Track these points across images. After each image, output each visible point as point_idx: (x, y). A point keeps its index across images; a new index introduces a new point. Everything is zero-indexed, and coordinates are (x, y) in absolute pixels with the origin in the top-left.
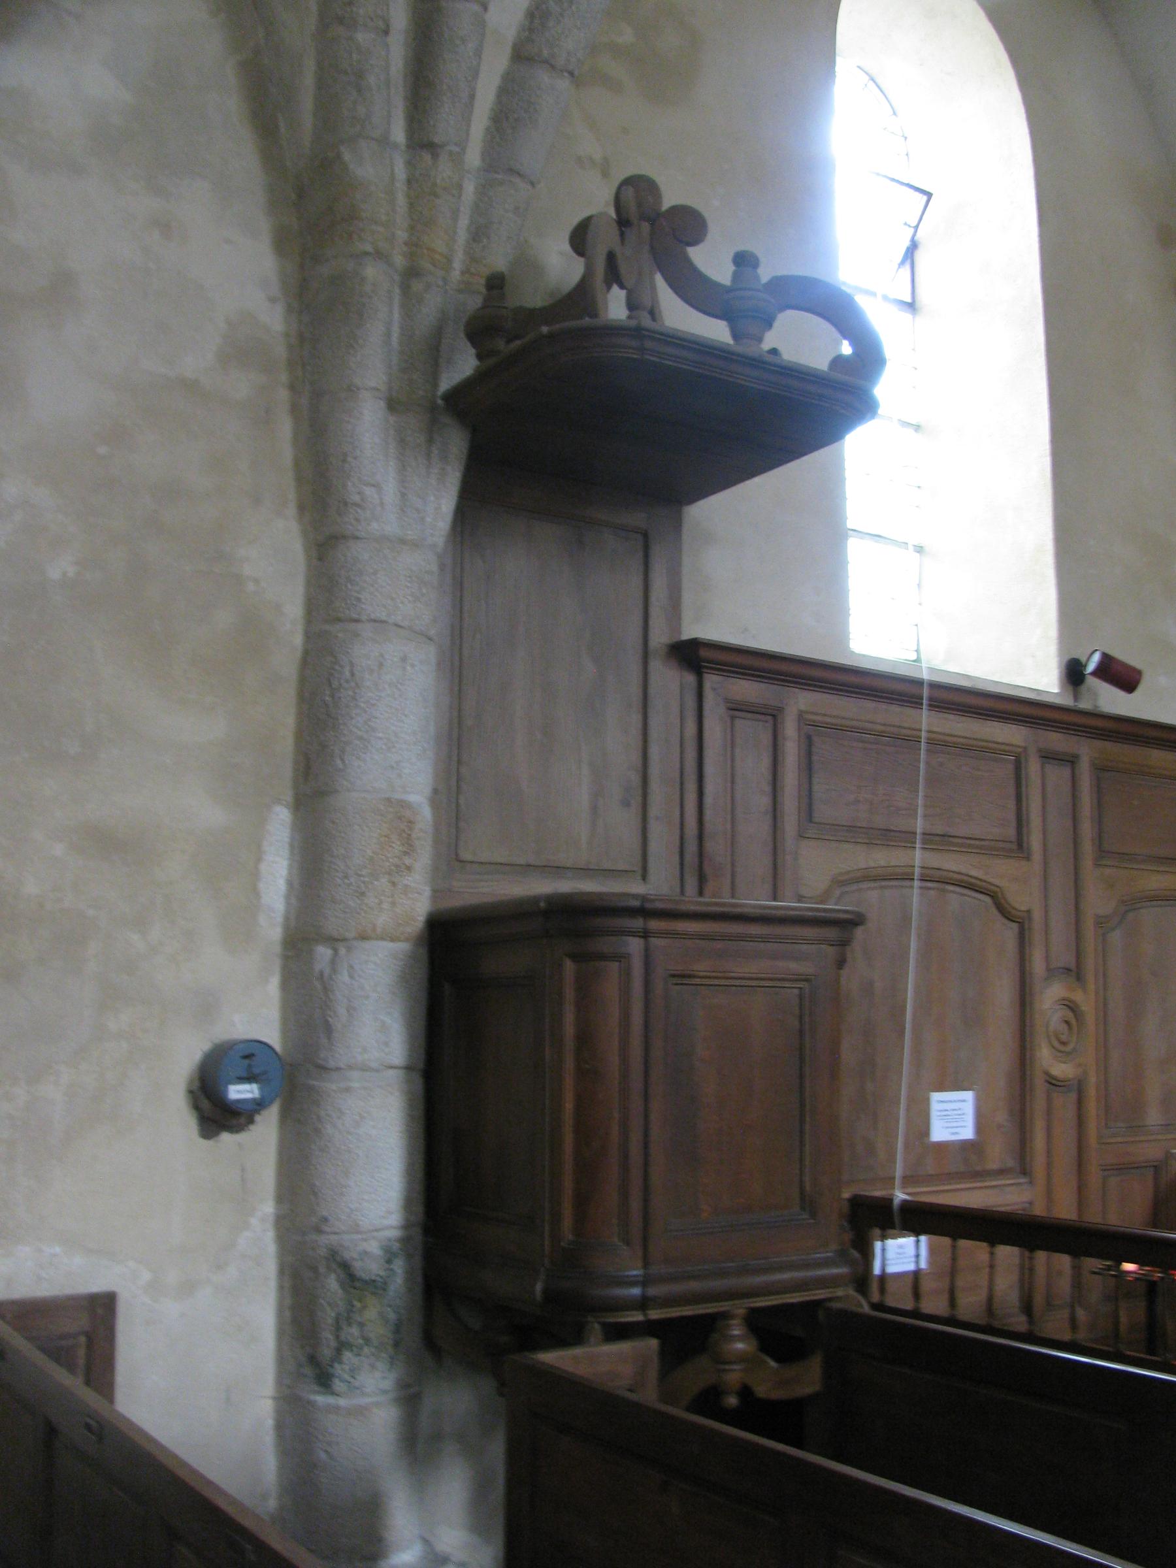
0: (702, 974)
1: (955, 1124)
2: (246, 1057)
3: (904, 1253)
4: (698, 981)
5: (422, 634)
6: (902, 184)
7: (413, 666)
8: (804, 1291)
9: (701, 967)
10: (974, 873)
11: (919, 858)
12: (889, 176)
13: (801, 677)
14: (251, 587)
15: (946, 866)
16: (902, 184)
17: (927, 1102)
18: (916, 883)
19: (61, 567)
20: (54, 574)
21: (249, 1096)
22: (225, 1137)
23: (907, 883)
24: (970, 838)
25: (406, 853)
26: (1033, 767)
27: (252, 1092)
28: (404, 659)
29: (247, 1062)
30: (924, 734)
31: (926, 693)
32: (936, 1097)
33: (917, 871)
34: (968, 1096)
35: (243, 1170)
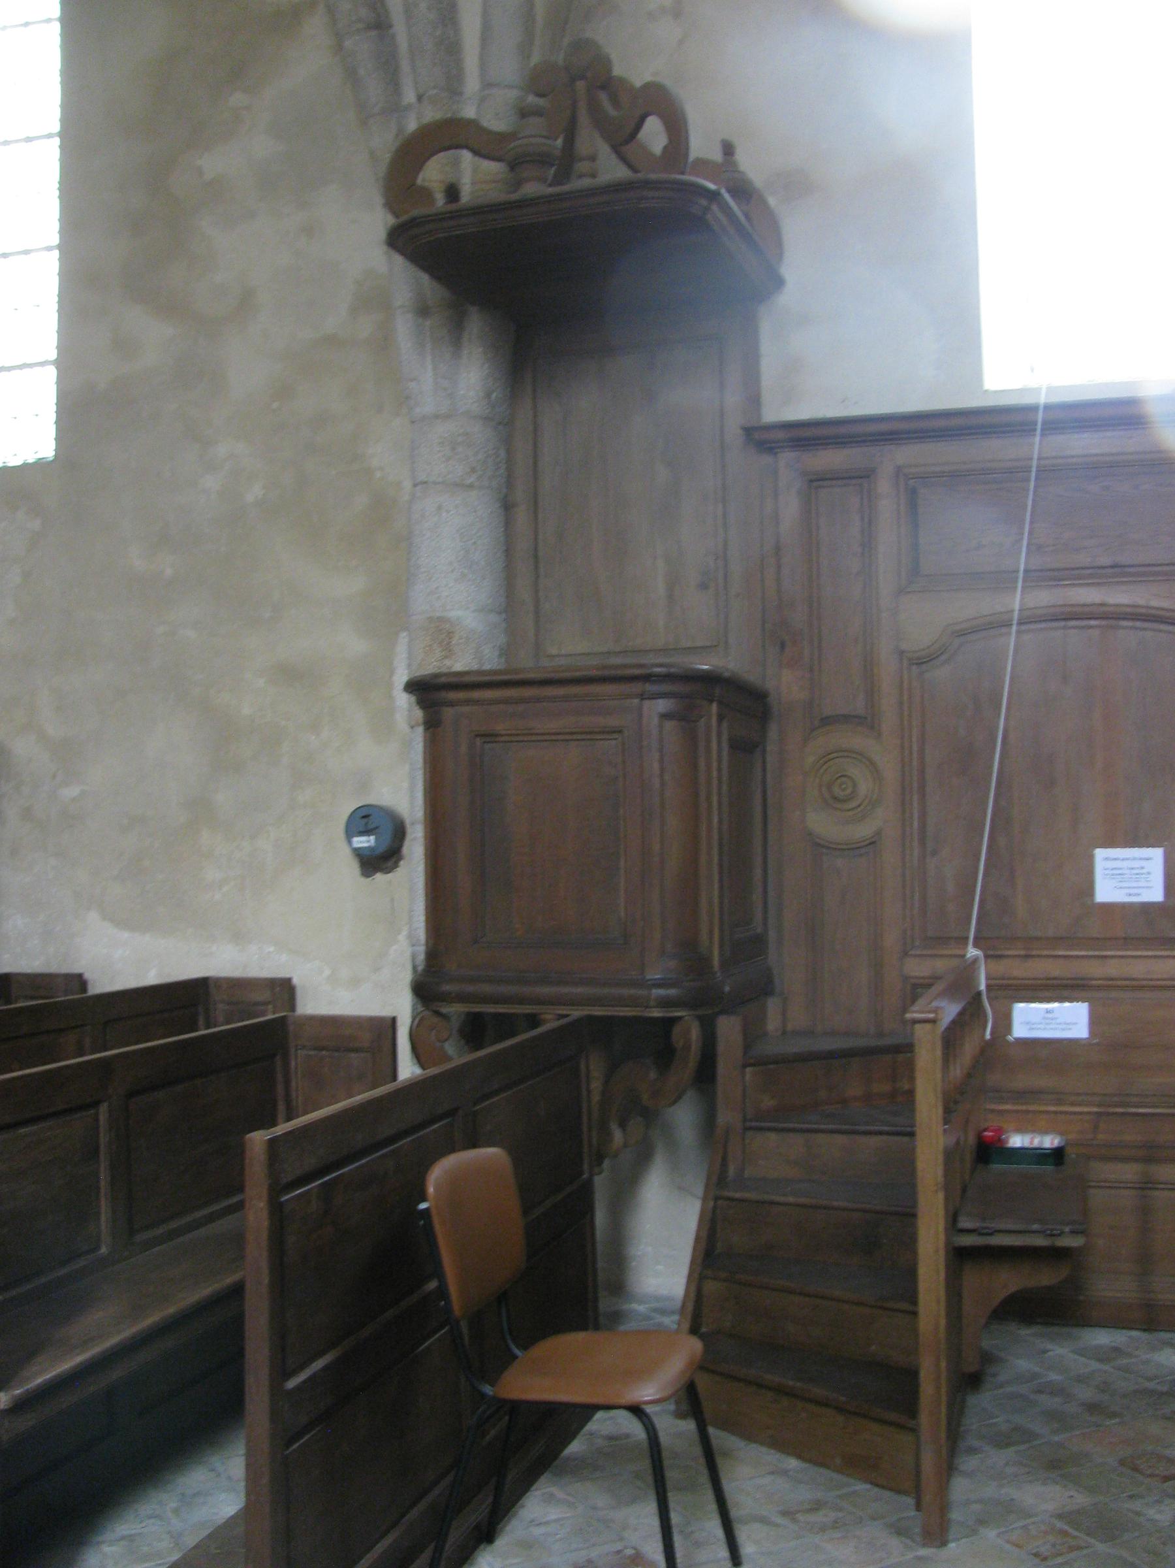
0: (504, 732)
1: (1135, 884)
2: (364, 817)
3: (1056, 1018)
4: (503, 739)
5: (456, 485)
6: (17, 26)
7: (448, 512)
8: (470, 1003)
9: (500, 728)
10: (1154, 603)
11: (1016, 602)
12: (20, 23)
13: (819, 438)
14: (378, 474)
15: (1111, 600)
16: (17, 26)
17: (1091, 859)
18: (1014, 628)
19: (254, 493)
20: (250, 498)
21: (366, 845)
22: (379, 876)
23: (1004, 630)
24: (1154, 565)
25: (446, 657)
27: (368, 841)
28: (440, 508)
29: (365, 820)
30: (1035, 463)
31: (1040, 417)
32: (1100, 854)
33: (1016, 615)
34: (1156, 855)
35: (392, 900)
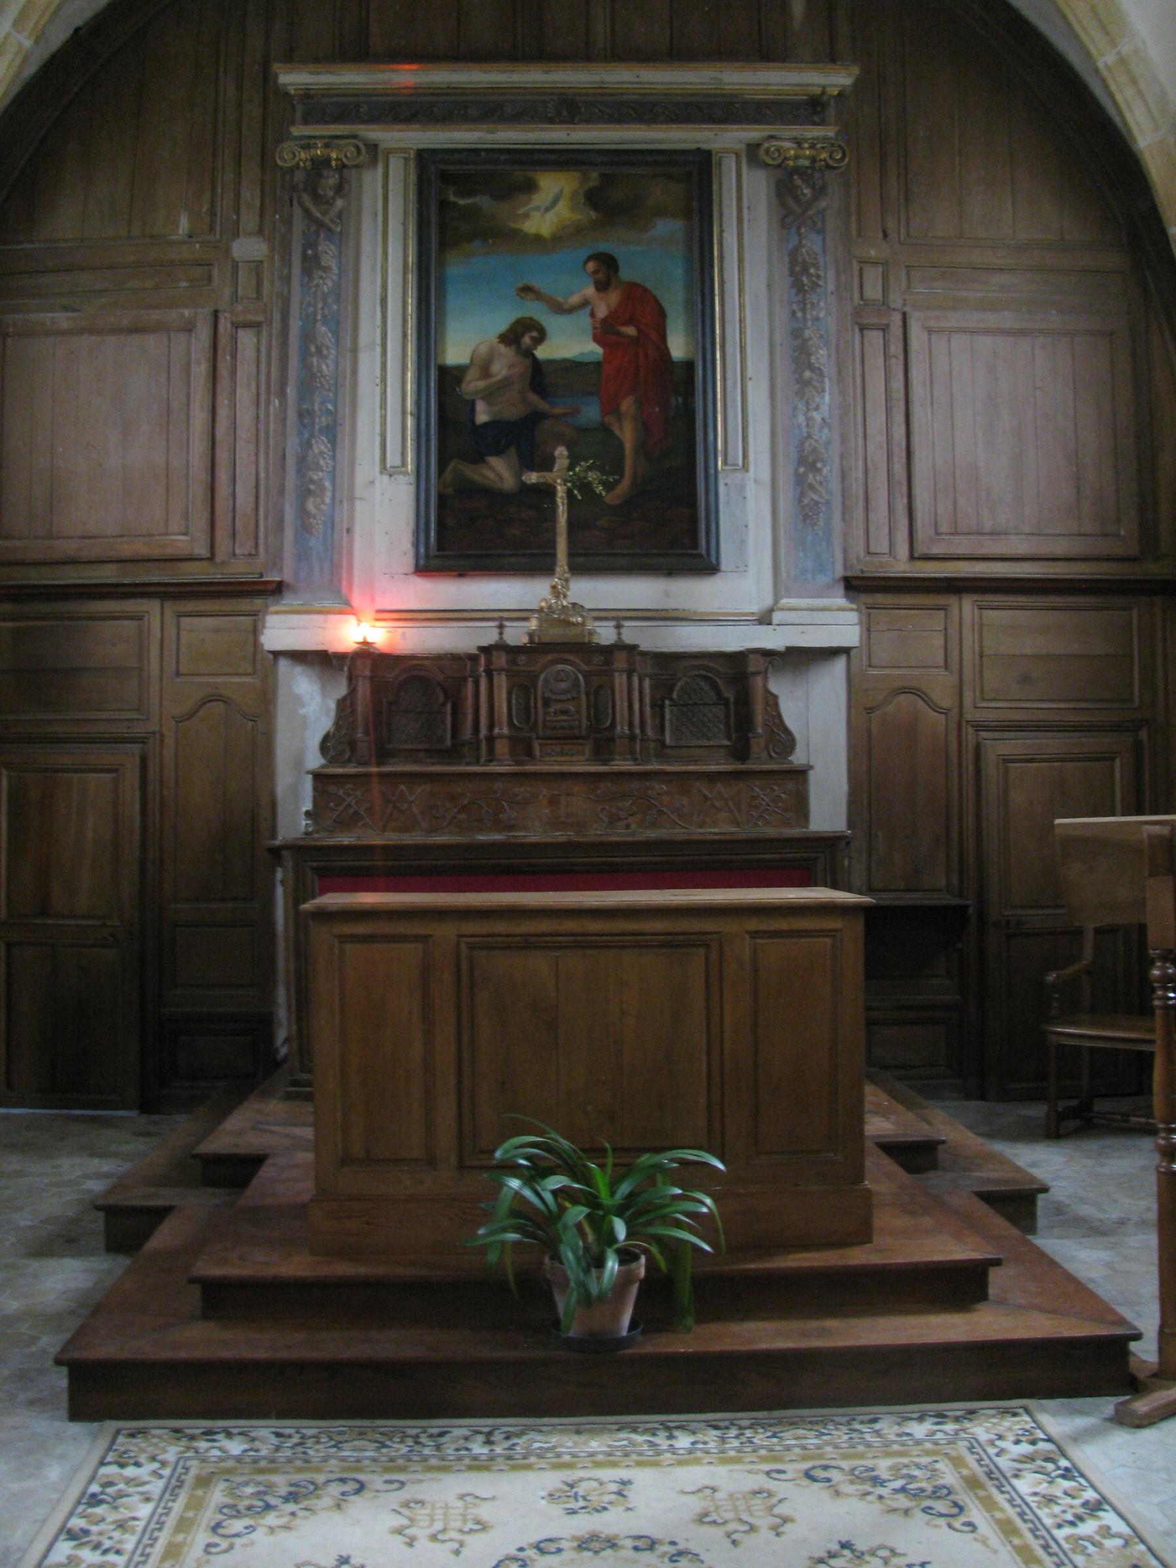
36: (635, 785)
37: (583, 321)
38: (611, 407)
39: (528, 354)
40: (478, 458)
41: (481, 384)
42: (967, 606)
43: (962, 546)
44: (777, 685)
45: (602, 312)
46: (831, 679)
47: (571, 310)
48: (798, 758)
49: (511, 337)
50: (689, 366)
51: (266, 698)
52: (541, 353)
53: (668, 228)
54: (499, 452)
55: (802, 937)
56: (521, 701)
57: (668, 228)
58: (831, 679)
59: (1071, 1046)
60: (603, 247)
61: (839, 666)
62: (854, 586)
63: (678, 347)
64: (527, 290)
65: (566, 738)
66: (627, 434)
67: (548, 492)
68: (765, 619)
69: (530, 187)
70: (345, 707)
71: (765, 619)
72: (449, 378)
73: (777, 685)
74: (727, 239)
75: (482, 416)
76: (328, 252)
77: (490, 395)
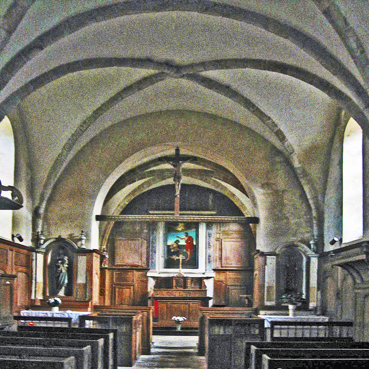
26: (9, 251)
36: (188, 292)
37: (184, 240)
38: (187, 250)
39: (177, 244)
40: (172, 256)
41: (172, 247)
42: (228, 273)
43: (228, 266)
44: (205, 281)
45: (186, 239)
46: (212, 280)
47: (183, 239)
48: (207, 289)
49: (175, 242)
50: (196, 245)
51: (147, 281)
52: (179, 244)
53: (194, 230)
54: (174, 255)
55: (218, 305)
56: (299, 320)
57: (194, 230)
58: (212, 280)
59: (146, 10)
60: (186, 232)
61: (212, 279)
62: (214, 270)
63: (195, 243)
64: (178, 237)
65: (181, 287)
66: (189, 253)
67: (179, 259)
68: (204, 274)
69: (179, 225)
70: (156, 282)
71: (204, 274)
72: (169, 246)
73: (205, 281)
74: (200, 230)
75: (172, 251)
76: (155, 233)
77: (173, 248)
